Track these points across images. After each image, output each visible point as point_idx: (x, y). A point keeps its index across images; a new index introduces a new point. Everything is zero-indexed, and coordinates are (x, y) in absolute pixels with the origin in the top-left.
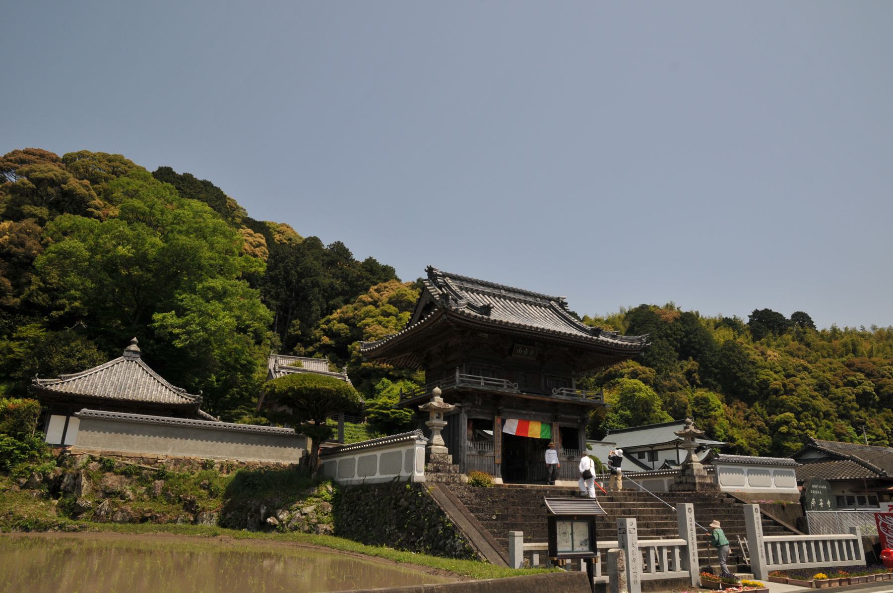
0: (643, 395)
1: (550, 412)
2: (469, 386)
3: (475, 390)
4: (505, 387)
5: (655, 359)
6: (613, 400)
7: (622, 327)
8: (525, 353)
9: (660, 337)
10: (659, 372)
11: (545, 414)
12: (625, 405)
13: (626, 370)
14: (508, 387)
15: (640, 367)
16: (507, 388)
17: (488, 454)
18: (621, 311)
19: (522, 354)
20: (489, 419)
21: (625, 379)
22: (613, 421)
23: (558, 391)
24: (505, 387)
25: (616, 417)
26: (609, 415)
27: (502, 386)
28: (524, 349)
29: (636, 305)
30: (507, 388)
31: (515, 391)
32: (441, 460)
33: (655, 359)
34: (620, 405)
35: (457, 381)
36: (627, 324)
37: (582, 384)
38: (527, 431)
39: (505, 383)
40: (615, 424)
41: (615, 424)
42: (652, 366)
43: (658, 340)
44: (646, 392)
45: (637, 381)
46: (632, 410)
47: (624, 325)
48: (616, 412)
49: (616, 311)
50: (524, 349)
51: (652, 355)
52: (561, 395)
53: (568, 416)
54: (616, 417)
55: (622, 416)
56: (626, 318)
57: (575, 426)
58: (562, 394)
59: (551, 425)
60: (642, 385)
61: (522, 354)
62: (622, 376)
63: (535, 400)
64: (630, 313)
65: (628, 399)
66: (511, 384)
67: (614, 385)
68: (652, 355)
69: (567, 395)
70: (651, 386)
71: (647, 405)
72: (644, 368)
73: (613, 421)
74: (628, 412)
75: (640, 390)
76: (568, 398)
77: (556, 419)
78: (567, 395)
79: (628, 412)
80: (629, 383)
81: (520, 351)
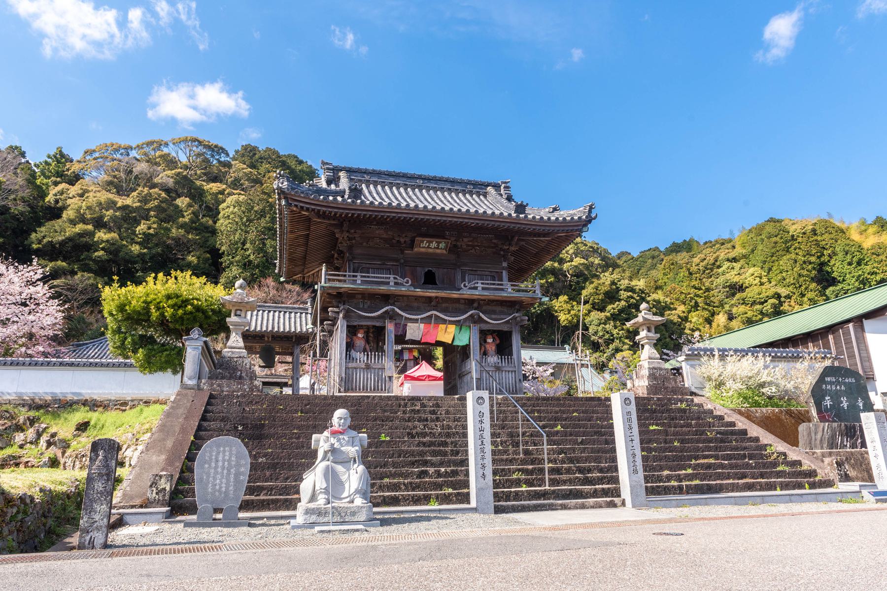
4: (392, 284)
14: (396, 284)
24: (392, 284)
39: (392, 279)
58: (476, 288)
61: (428, 247)
66: (400, 280)
69: (483, 289)
76: (486, 293)
78: (483, 289)
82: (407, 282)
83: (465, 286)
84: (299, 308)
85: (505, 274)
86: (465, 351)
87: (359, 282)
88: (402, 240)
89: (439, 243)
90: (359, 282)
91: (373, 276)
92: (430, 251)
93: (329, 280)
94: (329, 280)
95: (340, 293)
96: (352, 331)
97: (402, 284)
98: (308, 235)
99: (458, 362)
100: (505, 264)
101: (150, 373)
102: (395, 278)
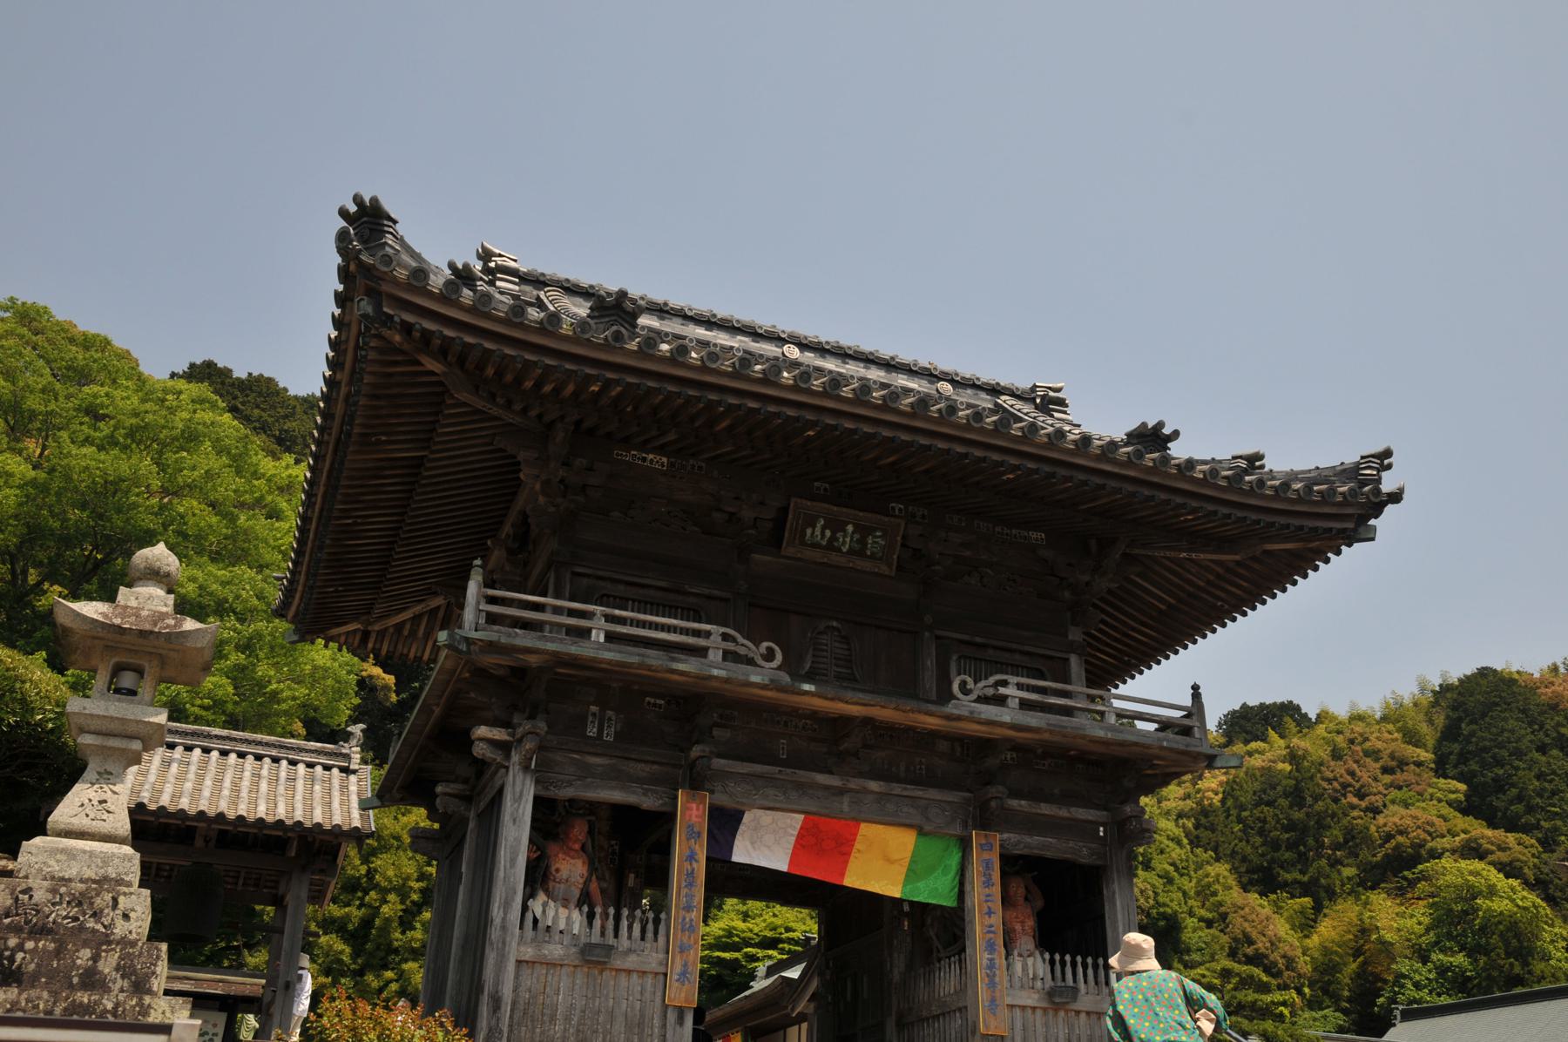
0: (1500, 905)
1: (965, 780)
2: (523, 639)
3: (560, 660)
4: (715, 656)
5: (1530, 809)
6: (1410, 923)
7: (1424, 728)
8: (847, 540)
9: (1542, 749)
10: (1548, 844)
11: (933, 794)
12: (1450, 936)
13: (1446, 842)
14: (728, 656)
15: (1489, 833)
16: (718, 656)
17: (631, 961)
18: (1422, 690)
19: (831, 546)
20: (649, 802)
21: (1446, 862)
22: (1417, 986)
23: (984, 687)
24: (715, 656)
25: (1425, 973)
26: (1403, 966)
27: (701, 652)
28: (836, 526)
29: (1459, 669)
30: (718, 656)
31: (762, 674)
32: (60, 914)
33: (1530, 809)
34: (1432, 937)
35: (469, 615)
36: (1440, 720)
37: (1314, 881)
38: (842, 875)
39: (715, 639)
40: (1424, 994)
41: (1424, 994)
42: (1526, 829)
43: (1537, 755)
44: (1509, 898)
45: (1477, 865)
46: (1472, 953)
47: (1431, 722)
48: (1425, 960)
49: (1407, 691)
50: (836, 526)
51: (1520, 798)
52: (996, 705)
53: (1046, 809)
54: (1425, 973)
55: (1442, 970)
56: (1435, 704)
57: (1080, 851)
58: (1001, 701)
59: (965, 845)
60: (1496, 877)
61: (831, 546)
62: (1435, 855)
63: (867, 721)
64: (1445, 689)
65: (1457, 920)
66: (744, 646)
67: (1412, 884)
68: (1520, 798)
69: (1025, 705)
70: (1526, 883)
71: (1517, 936)
72: (1498, 834)
73: (1417, 986)
74: (1460, 959)
75: (1492, 892)
76: (1033, 719)
77: (984, 819)
78: (1025, 705)
79: (1460, 959)
80: (1453, 871)
81: (818, 532)
82: (769, 656)
83: (966, 692)
84: (184, 734)
85: (1075, 665)
86: (939, 931)
87: (598, 636)
88: (747, 514)
89: (863, 531)
90: (598, 636)
91: (668, 627)
92: (835, 558)
93: (492, 619)
94: (492, 619)
95: (520, 672)
96: (550, 821)
97: (750, 662)
98: (419, 463)
99: (897, 967)
100: (1075, 635)
101: (46, 310)
102: (725, 637)
